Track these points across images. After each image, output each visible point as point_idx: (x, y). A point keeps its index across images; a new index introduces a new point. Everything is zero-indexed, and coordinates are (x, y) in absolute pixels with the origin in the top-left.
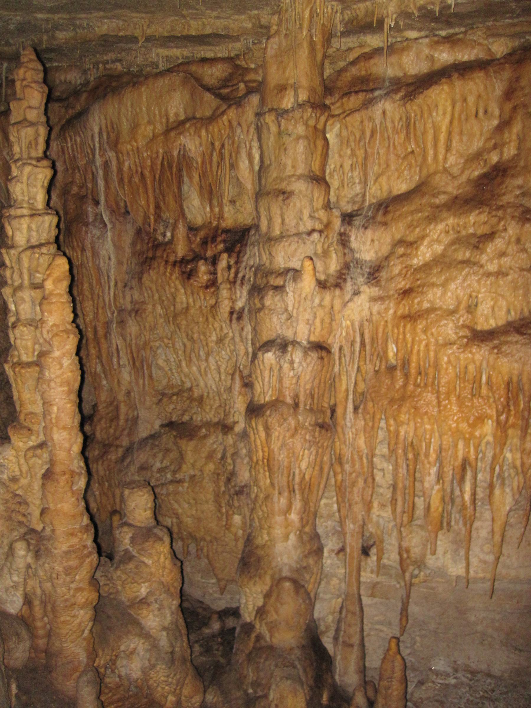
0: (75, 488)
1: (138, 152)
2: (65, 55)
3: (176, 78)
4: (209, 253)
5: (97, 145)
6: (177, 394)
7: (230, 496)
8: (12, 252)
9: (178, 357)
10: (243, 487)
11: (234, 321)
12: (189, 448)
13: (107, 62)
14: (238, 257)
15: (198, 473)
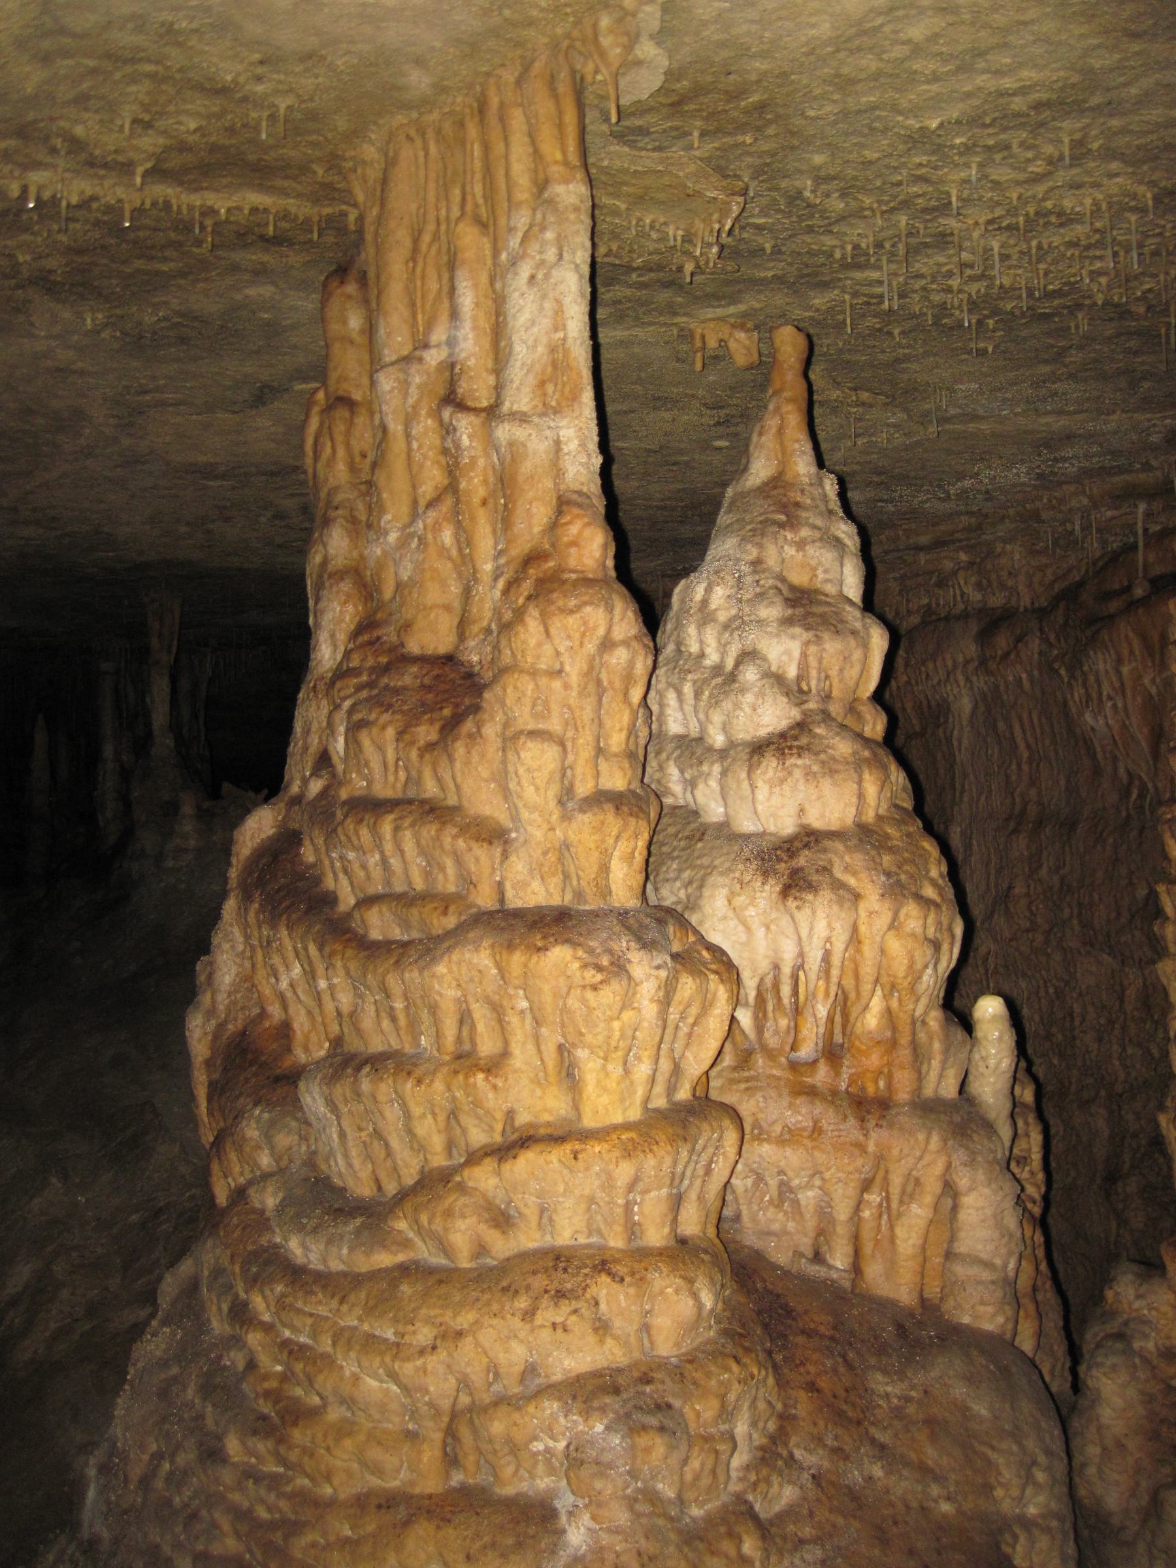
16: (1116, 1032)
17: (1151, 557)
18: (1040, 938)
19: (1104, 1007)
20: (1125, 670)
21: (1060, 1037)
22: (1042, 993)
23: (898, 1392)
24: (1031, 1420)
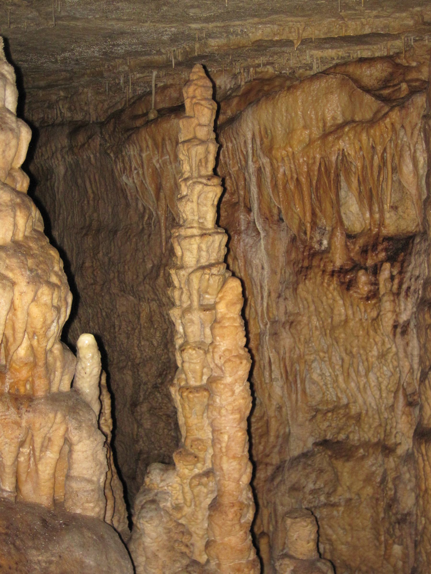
0: (243, 521)
1: (294, 158)
2: (216, 61)
3: (333, 81)
4: (370, 262)
5: (250, 151)
6: (332, 411)
7: (390, 524)
8: (182, 273)
9: (334, 371)
10: (406, 515)
11: (398, 336)
12: (346, 470)
13: (259, 66)
14: (402, 267)
15: (355, 497)
16: (136, 334)
17: (158, 99)
18: (98, 288)
19: (130, 321)
20: (144, 155)
21: (108, 337)
22: (99, 315)
23: (44, 558)
24: (116, 562)
